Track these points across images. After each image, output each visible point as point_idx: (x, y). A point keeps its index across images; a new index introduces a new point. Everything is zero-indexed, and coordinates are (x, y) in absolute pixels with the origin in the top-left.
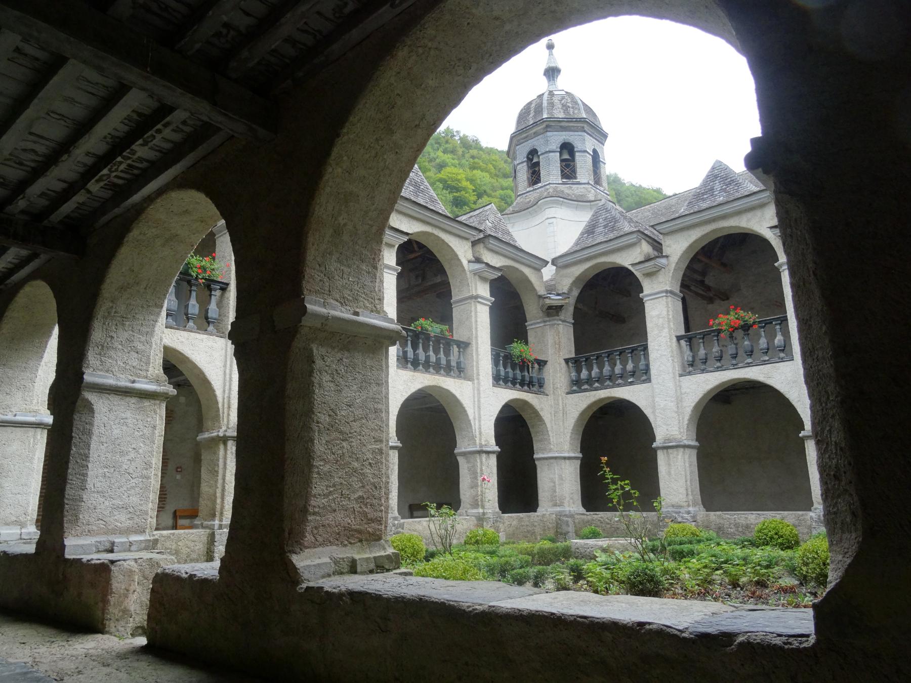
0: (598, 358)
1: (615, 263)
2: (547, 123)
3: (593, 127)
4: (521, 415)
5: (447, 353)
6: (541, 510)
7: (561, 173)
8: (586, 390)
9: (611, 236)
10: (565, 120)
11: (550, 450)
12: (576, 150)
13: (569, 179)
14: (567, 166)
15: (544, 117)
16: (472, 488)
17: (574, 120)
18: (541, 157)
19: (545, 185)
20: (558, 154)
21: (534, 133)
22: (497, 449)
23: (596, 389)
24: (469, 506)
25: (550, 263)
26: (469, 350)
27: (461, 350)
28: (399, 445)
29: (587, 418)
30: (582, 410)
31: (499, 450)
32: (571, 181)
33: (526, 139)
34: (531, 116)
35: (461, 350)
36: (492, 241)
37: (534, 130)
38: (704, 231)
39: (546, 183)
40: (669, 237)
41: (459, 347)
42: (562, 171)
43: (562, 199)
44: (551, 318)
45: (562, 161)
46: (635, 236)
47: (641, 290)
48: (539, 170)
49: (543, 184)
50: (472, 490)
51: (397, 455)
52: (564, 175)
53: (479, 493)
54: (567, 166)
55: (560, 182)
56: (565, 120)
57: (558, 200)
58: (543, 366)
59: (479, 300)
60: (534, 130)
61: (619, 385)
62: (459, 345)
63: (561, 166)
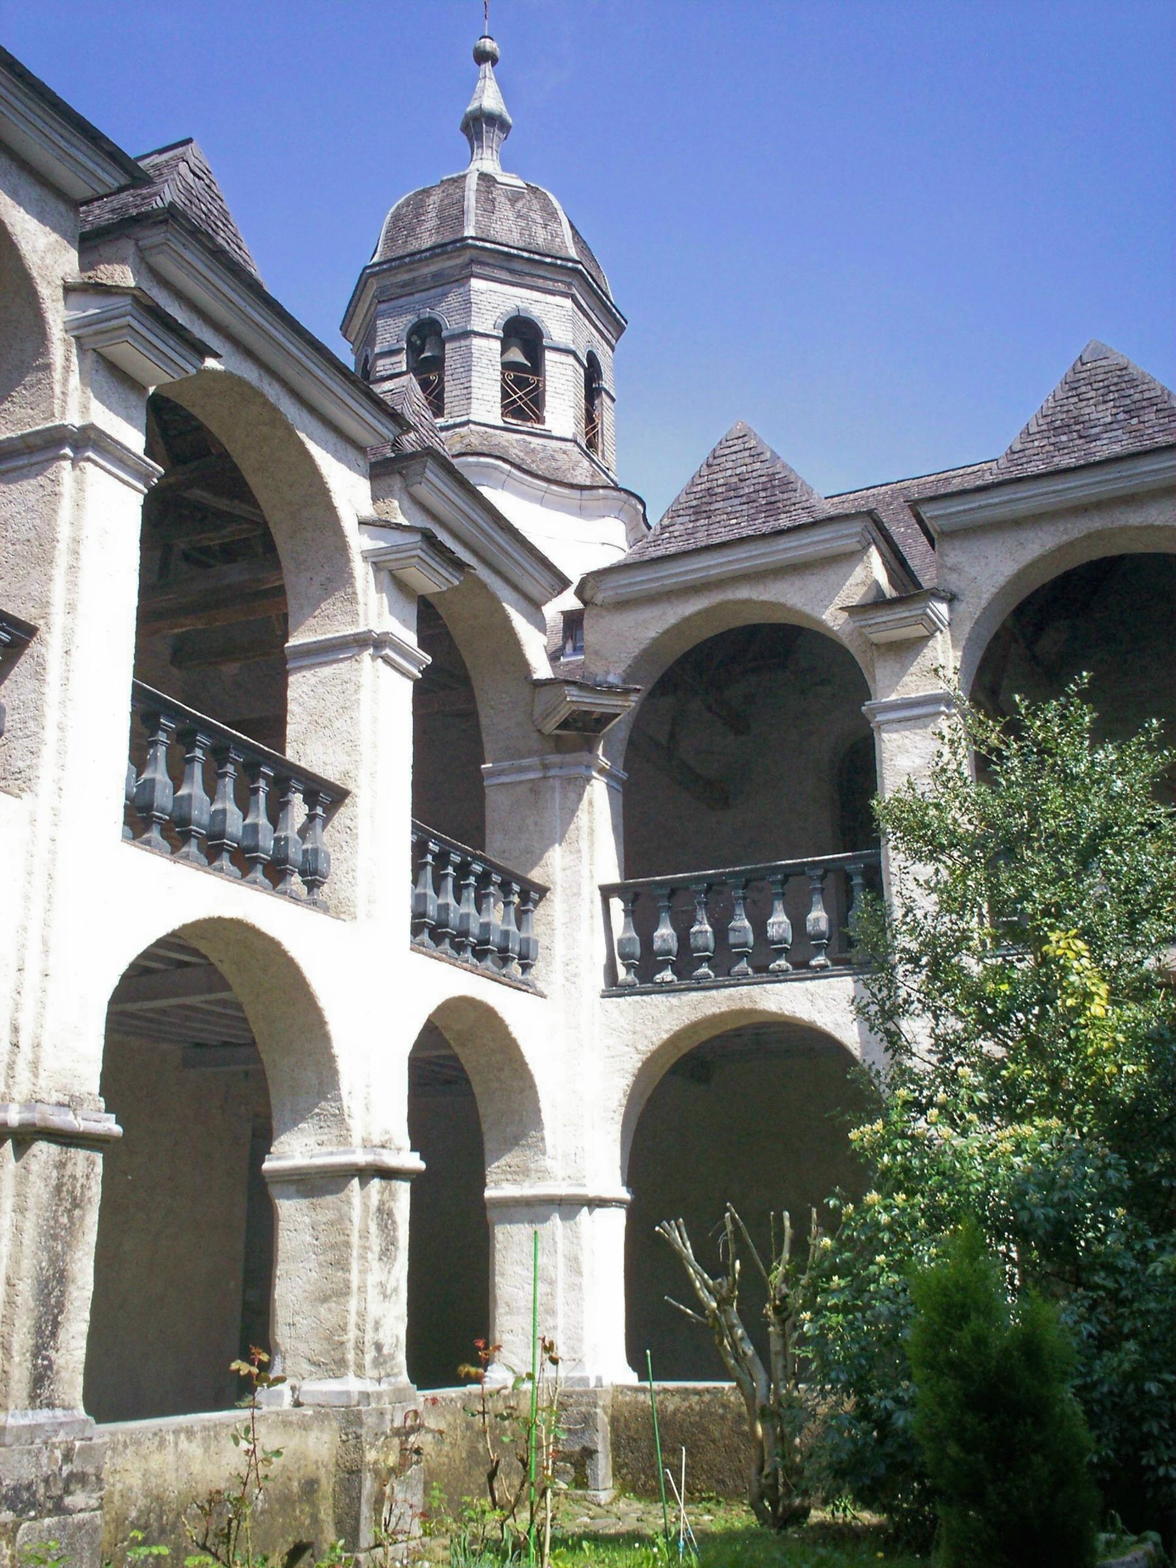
0: (673, 893)
1: (782, 606)
2: (474, 252)
3: (596, 293)
4: (455, 1058)
5: (277, 810)
6: (497, 1376)
7: (503, 399)
8: (666, 989)
9: (764, 525)
10: (525, 254)
11: (544, 1174)
12: (545, 342)
13: (524, 420)
14: (520, 383)
15: (466, 234)
16: (325, 1299)
17: (548, 260)
18: (447, 346)
19: (456, 426)
20: (497, 345)
21: (435, 275)
22: (414, 1161)
23: (702, 986)
24: (306, 1367)
25: (572, 589)
26: (342, 816)
27: (319, 810)
28: (110, 1125)
29: (659, 1072)
30: (652, 1048)
31: (422, 1166)
32: (527, 426)
33: (409, 289)
34: (428, 225)
35: (319, 810)
36: (432, 474)
37: (433, 268)
38: (1066, 531)
39: (458, 420)
40: (957, 544)
41: (311, 799)
42: (505, 395)
43: (507, 467)
44: (569, 758)
45: (507, 366)
46: (856, 527)
47: (865, 693)
48: (441, 381)
49: (451, 422)
50: (322, 1310)
51: (99, 1169)
52: (510, 408)
53: (353, 1319)
54: (520, 383)
55: (502, 424)
56: (525, 254)
57: (496, 468)
58: (536, 903)
59: (388, 651)
60: (433, 268)
61: (779, 977)
62: (317, 793)
63: (503, 380)
